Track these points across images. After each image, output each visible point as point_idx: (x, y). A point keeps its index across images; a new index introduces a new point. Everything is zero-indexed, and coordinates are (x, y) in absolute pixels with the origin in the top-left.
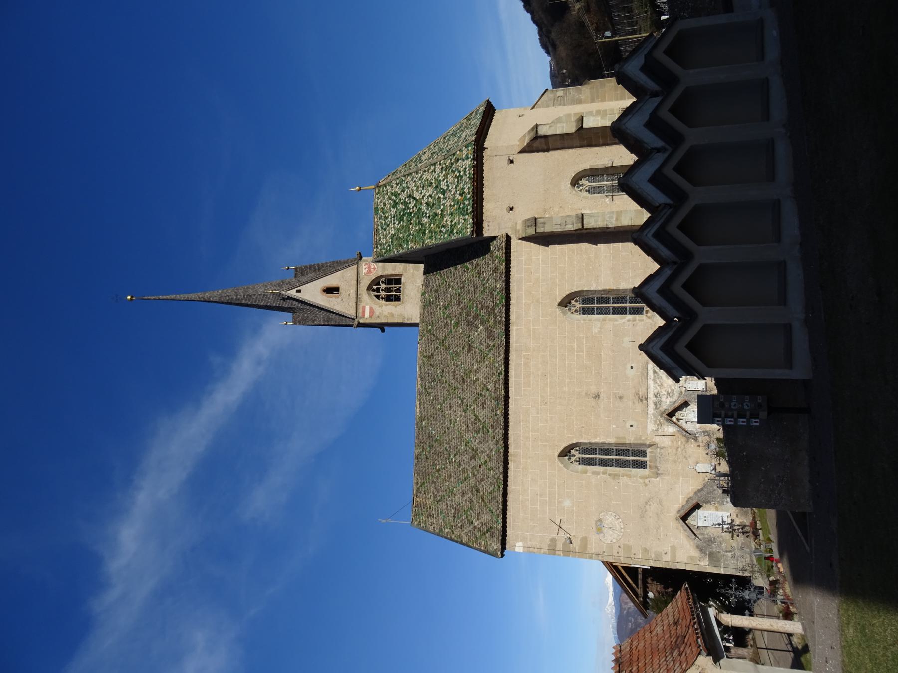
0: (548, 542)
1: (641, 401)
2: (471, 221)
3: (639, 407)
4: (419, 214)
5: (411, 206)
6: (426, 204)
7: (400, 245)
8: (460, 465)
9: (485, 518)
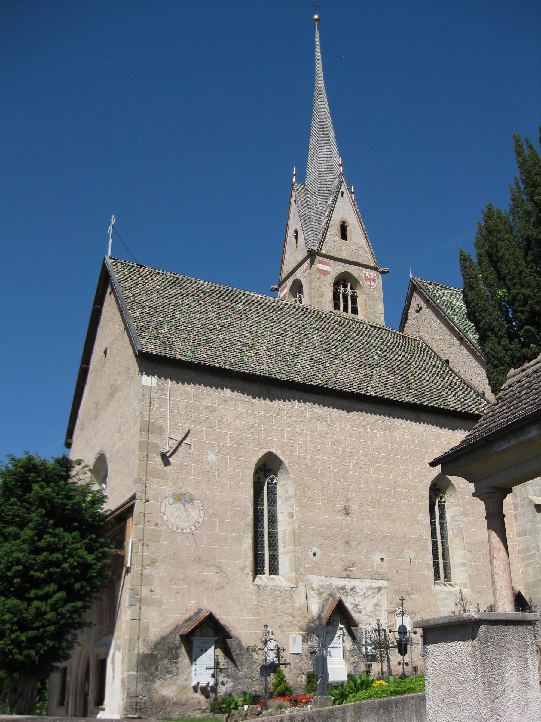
0: (159, 422)
1: (346, 570)
3: (337, 566)
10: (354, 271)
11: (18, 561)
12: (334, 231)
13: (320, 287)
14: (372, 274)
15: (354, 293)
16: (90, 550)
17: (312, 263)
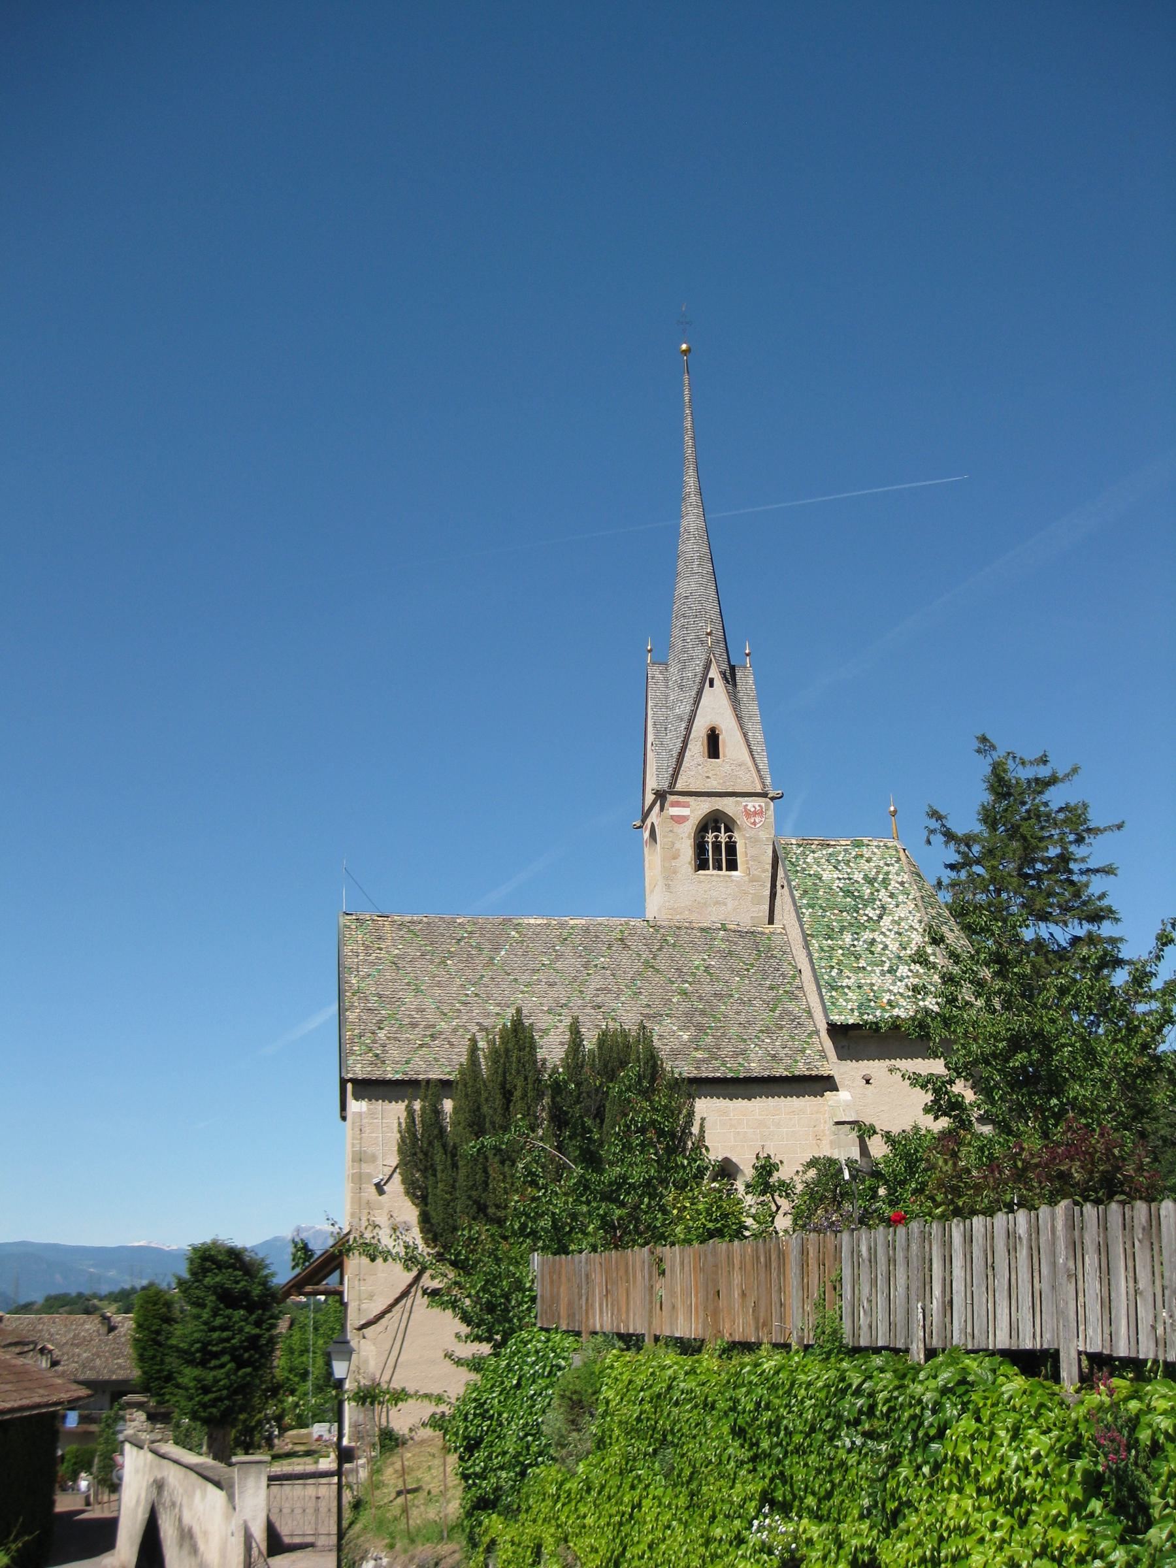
0: (370, 1150)
2: (851, 1022)
4: (857, 928)
5: (869, 911)
6: (874, 940)
7: (805, 892)
8: (465, 1004)
9: (394, 1052)
10: (728, 806)
11: (198, 1341)
12: (697, 746)
13: (673, 843)
14: (757, 805)
15: (730, 837)
16: (258, 1324)
17: (662, 809)
